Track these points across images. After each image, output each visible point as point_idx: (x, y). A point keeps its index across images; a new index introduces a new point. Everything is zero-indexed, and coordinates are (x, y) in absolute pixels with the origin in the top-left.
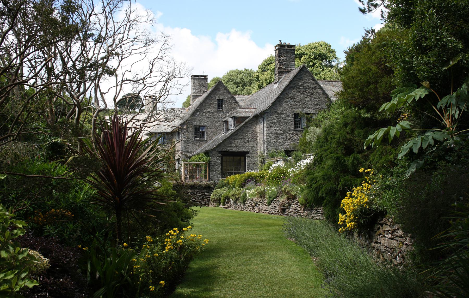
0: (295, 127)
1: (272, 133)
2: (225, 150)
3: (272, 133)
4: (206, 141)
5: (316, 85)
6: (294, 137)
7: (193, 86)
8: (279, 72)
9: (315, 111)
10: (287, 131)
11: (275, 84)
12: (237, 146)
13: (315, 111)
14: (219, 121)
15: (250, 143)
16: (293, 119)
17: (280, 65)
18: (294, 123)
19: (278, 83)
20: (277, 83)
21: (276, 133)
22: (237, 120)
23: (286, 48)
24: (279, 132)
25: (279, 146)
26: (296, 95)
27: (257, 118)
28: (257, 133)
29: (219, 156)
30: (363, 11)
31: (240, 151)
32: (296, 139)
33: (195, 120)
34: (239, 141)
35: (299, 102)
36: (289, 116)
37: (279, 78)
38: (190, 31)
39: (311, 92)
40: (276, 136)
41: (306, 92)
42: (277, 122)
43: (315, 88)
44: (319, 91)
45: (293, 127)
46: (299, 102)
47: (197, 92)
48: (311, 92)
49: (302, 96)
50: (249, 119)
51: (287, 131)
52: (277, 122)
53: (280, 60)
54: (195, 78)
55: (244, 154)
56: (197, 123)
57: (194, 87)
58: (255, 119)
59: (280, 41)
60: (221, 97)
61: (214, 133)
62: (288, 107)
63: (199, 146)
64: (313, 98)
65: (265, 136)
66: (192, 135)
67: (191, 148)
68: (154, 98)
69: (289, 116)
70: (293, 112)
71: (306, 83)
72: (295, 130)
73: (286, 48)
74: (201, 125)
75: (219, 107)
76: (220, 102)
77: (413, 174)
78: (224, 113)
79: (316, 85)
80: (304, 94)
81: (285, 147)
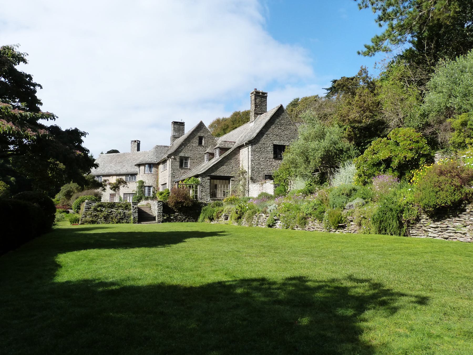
2: (213, 174)
10: (267, 159)
14: (200, 154)
17: (255, 108)
22: (223, 150)
23: (261, 94)
30: (359, 53)
33: (180, 152)
34: (225, 167)
37: (255, 118)
38: (64, 129)
45: (272, 156)
47: (177, 134)
50: (231, 150)
51: (267, 159)
54: (175, 123)
56: (182, 154)
57: (175, 130)
58: (238, 149)
63: (184, 173)
64: (287, 133)
65: (250, 163)
72: (274, 158)
75: (200, 143)
76: (201, 139)
77: (116, 289)
81: (266, 173)
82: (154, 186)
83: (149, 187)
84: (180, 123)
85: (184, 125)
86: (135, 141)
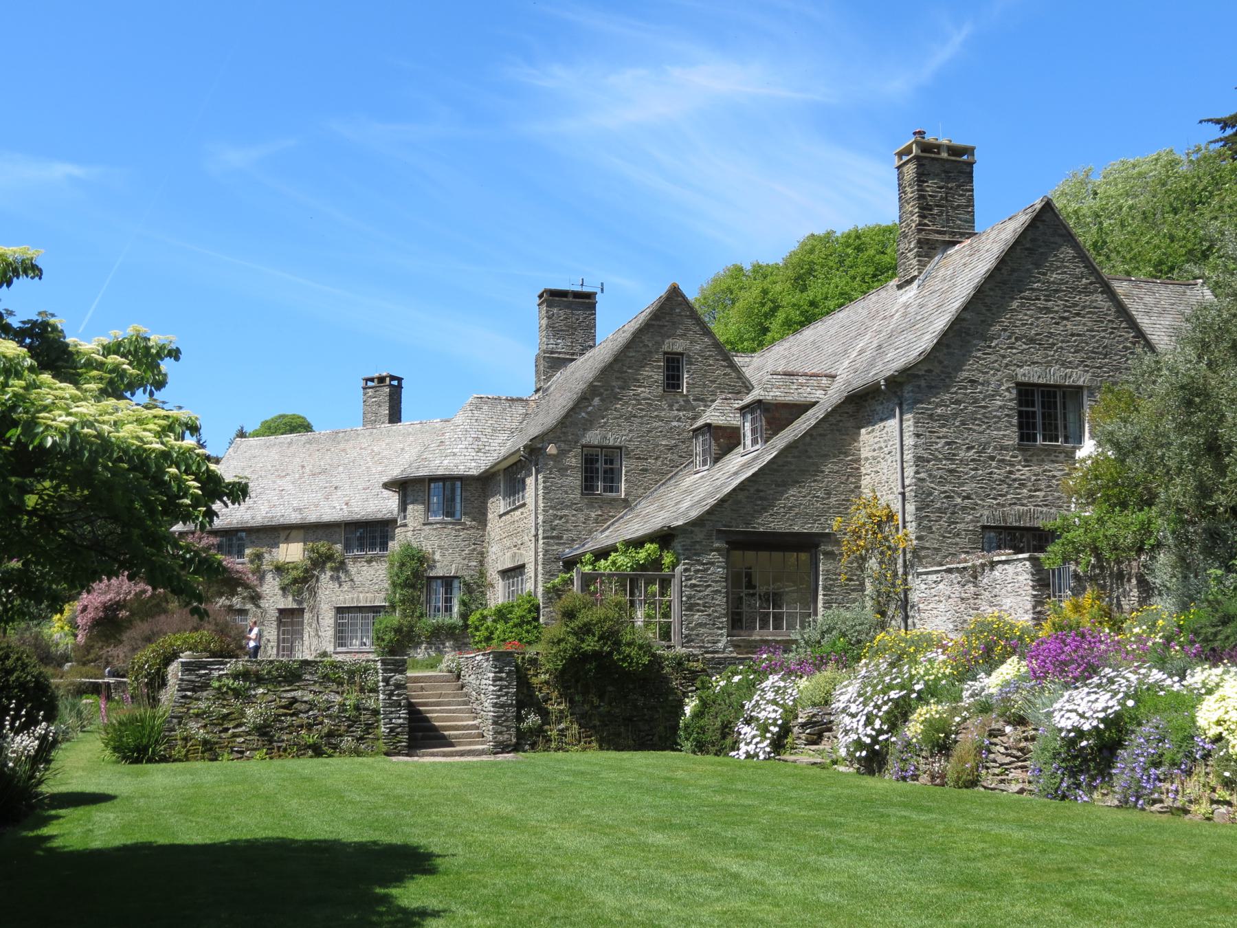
0: (1022, 438)
1: (936, 459)
3: (936, 459)
4: (625, 500)
5: (1092, 279)
6: (1017, 475)
7: (548, 326)
8: (919, 242)
9: (1088, 376)
11: (900, 287)
12: (788, 515)
13: (1088, 376)
15: (833, 500)
16: (1012, 404)
17: (922, 216)
18: (1015, 421)
19: (916, 283)
20: (909, 282)
21: (951, 458)
23: (944, 155)
24: (962, 454)
25: (964, 508)
26: (1022, 316)
27: (864, 405)
28: (858, 460)
29: (717, 550)
31: (796, 529)
32: (1023, 485)
33: (588, 425)
35: (1032, 341)
36: (996, 392)
37: (922, 265)
39: (1075, 305)
40: (951, 471)
41: (1057, 305)
42: (955, 416)
43: (1085, 291)
44: (1100, 300)
45: (1011, 436)
46: (1032, 341)
47: (561, 346)
48: (1075, 305)
49: (1046, 318)
52: (955, 416)
53: (921, 197)
54: (553, 298)
55: (809, 545)
56: (593, 437)
57: (553, 329)
58: (850, 409)
59: (921, 133)
60: (679, 345)
61: (656, 472)
62: (993, 358)
64: (1080, 329)
65: (910, 472)
66: (574, 480)
67: (569, 526)
68: (395, 383)
69: (996, 392)
70: (1011, 378)
71: (1061, 270)
73: (944, 155)
74: (606, 443)
76: (673, 369)
78: (687, 401)
79: (1092, 279)
80: (1048, 310)
82: (467, 575)
83: (448, 582)
84: (577, 295)
85: (592, 307)
86: (381, 380)
